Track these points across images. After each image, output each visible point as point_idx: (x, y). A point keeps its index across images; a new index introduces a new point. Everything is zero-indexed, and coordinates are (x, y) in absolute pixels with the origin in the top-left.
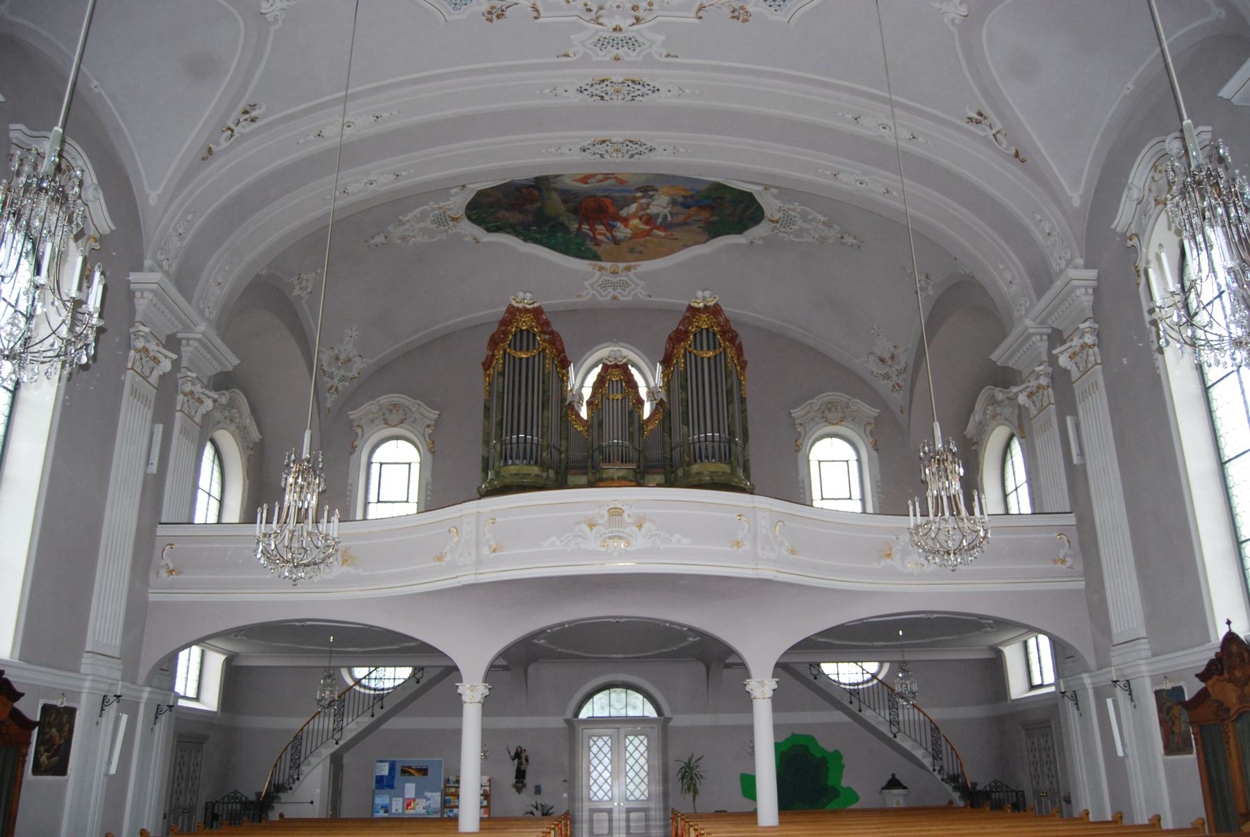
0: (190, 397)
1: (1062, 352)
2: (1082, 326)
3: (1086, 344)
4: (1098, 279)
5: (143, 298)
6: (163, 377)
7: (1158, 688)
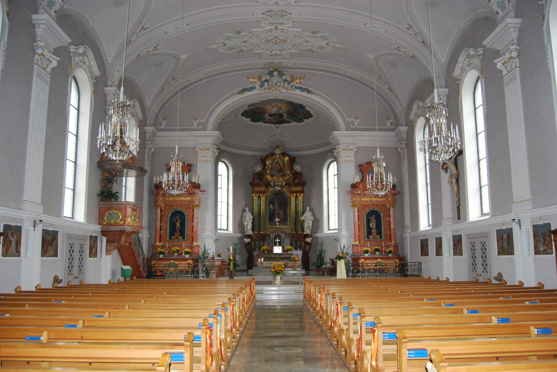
0: (42, 57)
1: (499, 61)
2: (511, 47)
3: (512, 56)
4: (449, 92)
5: (39, 28)
6: (53, 69)
7: (535, 224)
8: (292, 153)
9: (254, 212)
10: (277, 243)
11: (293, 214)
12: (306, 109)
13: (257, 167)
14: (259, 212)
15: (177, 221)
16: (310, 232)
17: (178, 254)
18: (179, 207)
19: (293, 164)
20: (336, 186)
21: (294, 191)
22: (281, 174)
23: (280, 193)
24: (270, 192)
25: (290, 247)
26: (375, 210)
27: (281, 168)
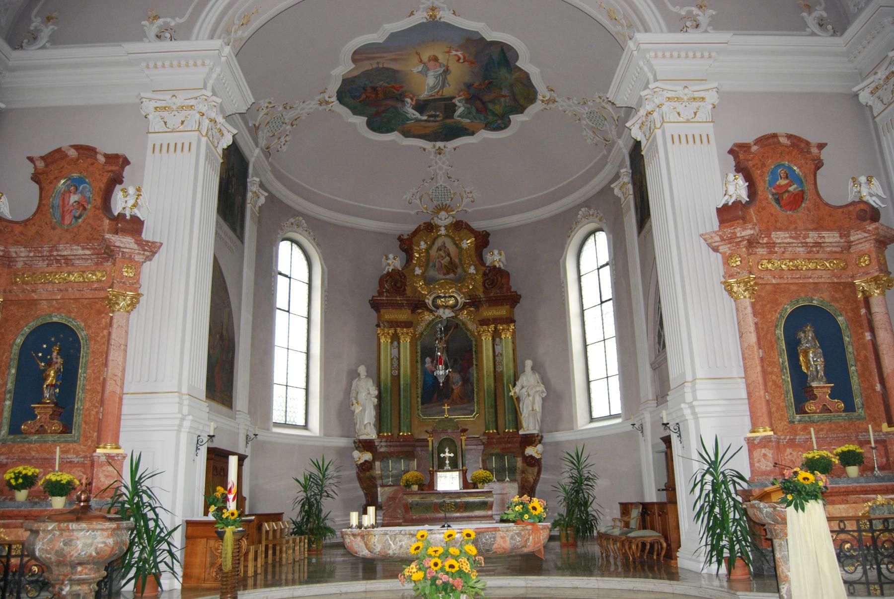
8: (479, 225)
9: (383, 377)
10: (447, 462)
11: (488, 382)
12: (519, 64)
13: (387, 259)
14: (396, 379)
15: (49, 364)
16: (537, 428)
17: (29, 497)
18: (58, 309)
19: (485, 250)
20: (608, 293)
21: (489, 320)
22: (452, 276)
23: (452, 326)
24: (423, 324)
25: (482, 473)
26: (815, 303)
27: (451, 262)
